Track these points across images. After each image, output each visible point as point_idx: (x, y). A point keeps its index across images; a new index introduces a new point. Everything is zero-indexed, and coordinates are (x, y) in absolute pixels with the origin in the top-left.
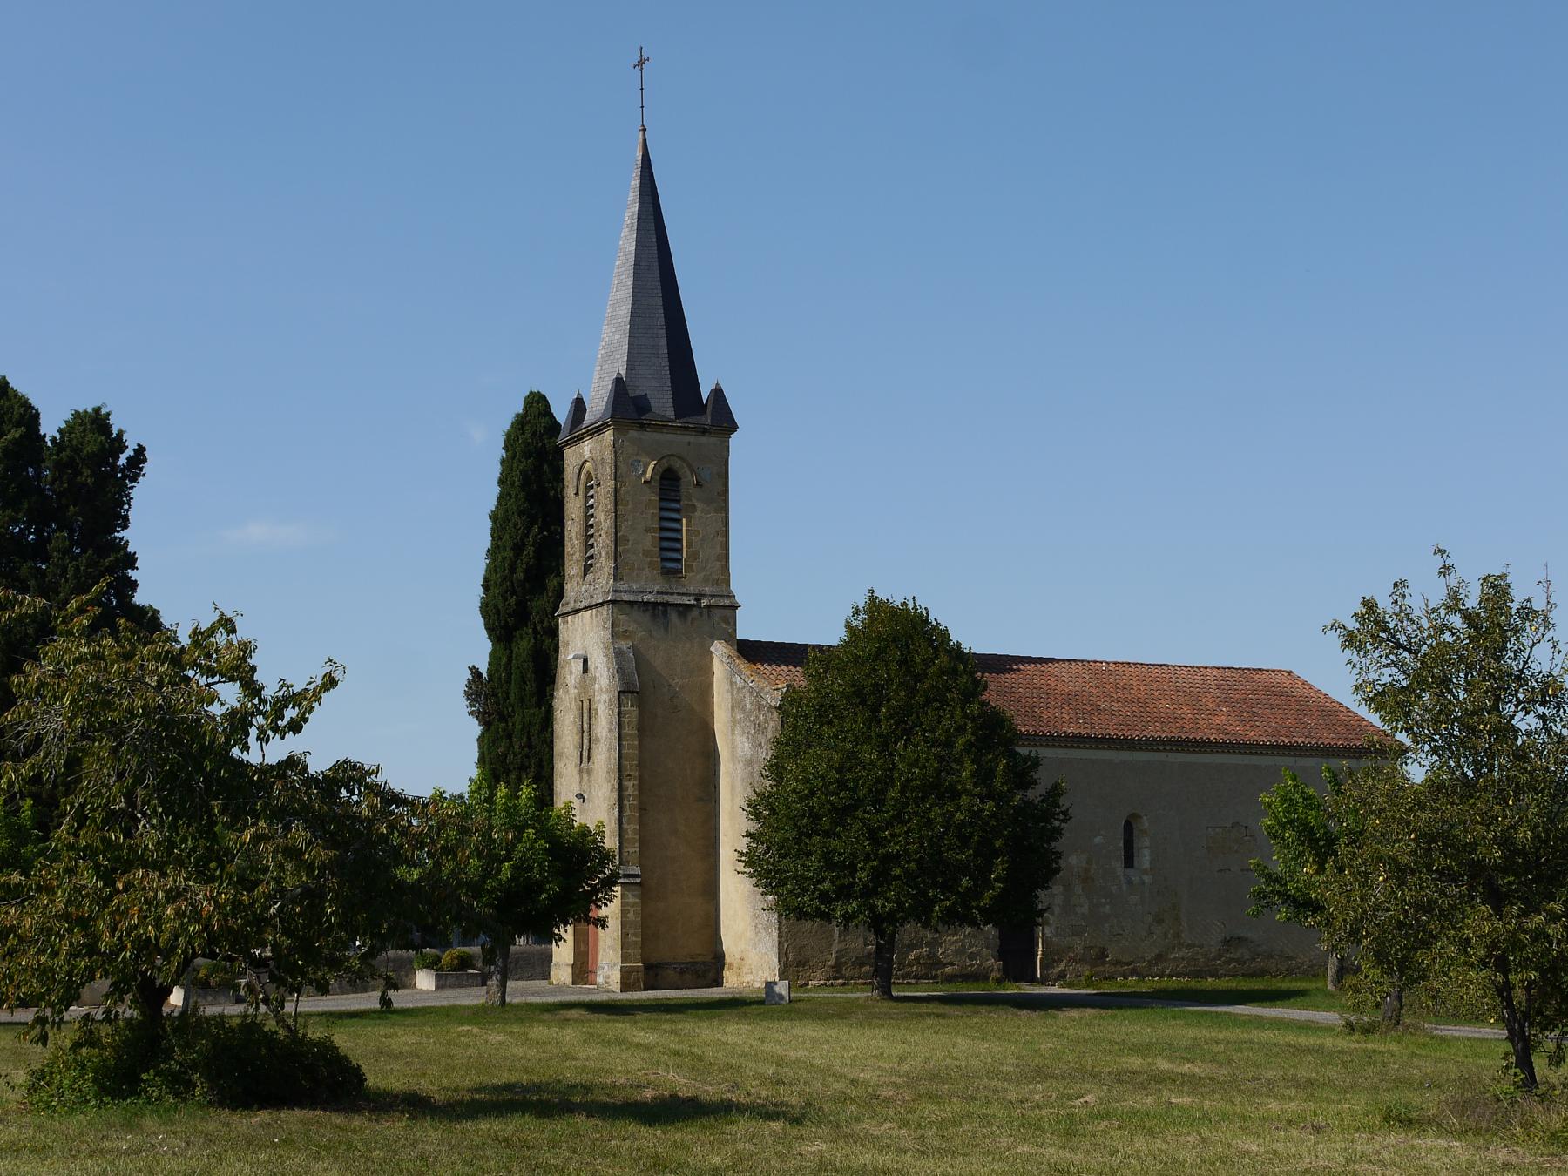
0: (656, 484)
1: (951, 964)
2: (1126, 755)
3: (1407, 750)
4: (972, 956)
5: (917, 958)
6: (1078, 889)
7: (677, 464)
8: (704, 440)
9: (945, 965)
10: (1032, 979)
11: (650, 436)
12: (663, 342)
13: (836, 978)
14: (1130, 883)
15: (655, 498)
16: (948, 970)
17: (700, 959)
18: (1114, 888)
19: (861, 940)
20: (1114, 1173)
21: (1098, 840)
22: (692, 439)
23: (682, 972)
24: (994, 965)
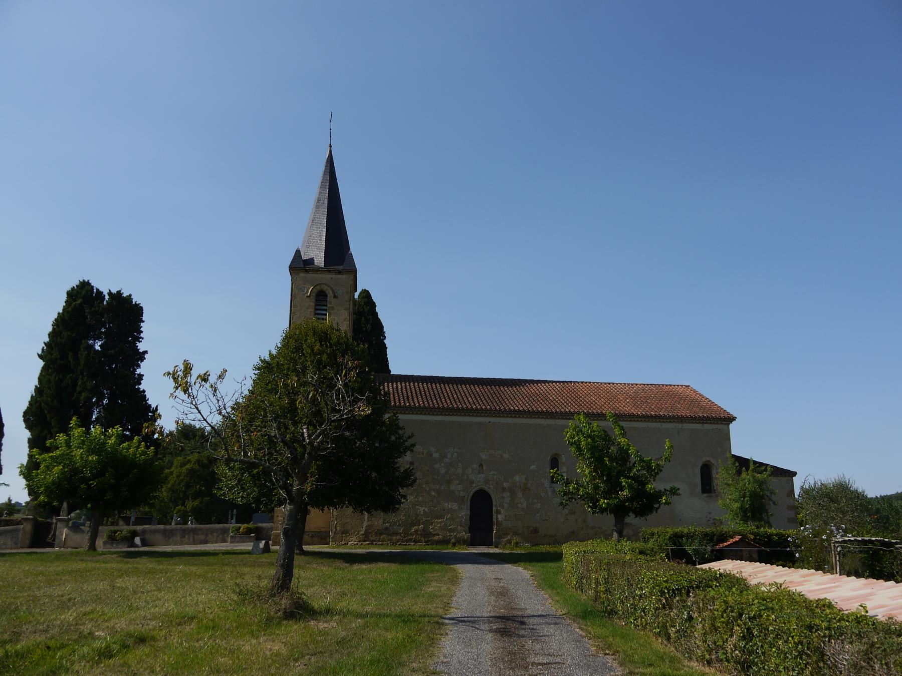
0: (313, 298)
1: (438, 535)
2: (657, 425)
3: (584, 413)
4: (451, 531)
5: (416, 531)
6: (520, 494)
7: (325, 288)
8: (339, 276)
9: (434, 535)
10: (489, 544)
11: (310, 276)
12: (324, 234)
13: (365, 541)
14: (554, 491)
15: (312, 304)
16: (436, 538)
17: (323, 530)
18: (543, 494)
19: (381, 521)
20: (335, 672)
21: (533, 467)
22: (333, 276)
23: (312, 536)
24: (466, 535)
